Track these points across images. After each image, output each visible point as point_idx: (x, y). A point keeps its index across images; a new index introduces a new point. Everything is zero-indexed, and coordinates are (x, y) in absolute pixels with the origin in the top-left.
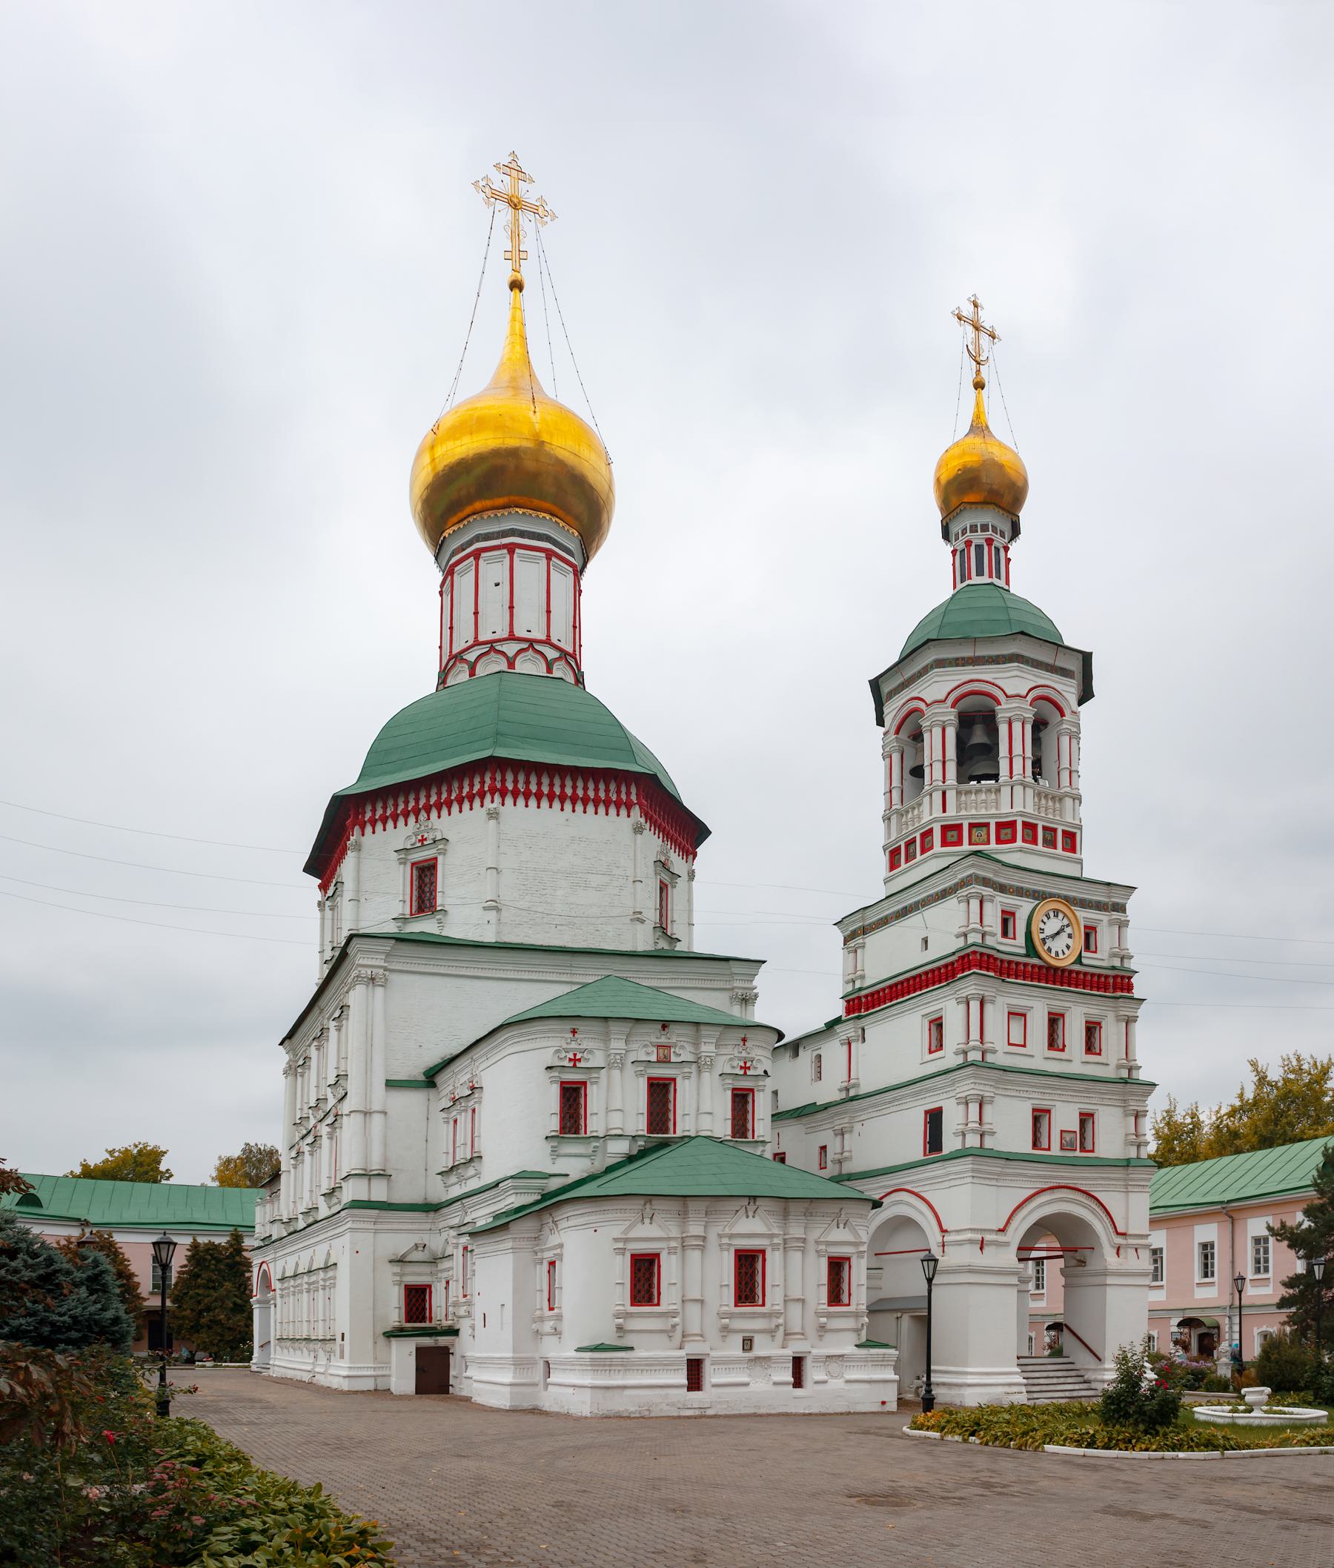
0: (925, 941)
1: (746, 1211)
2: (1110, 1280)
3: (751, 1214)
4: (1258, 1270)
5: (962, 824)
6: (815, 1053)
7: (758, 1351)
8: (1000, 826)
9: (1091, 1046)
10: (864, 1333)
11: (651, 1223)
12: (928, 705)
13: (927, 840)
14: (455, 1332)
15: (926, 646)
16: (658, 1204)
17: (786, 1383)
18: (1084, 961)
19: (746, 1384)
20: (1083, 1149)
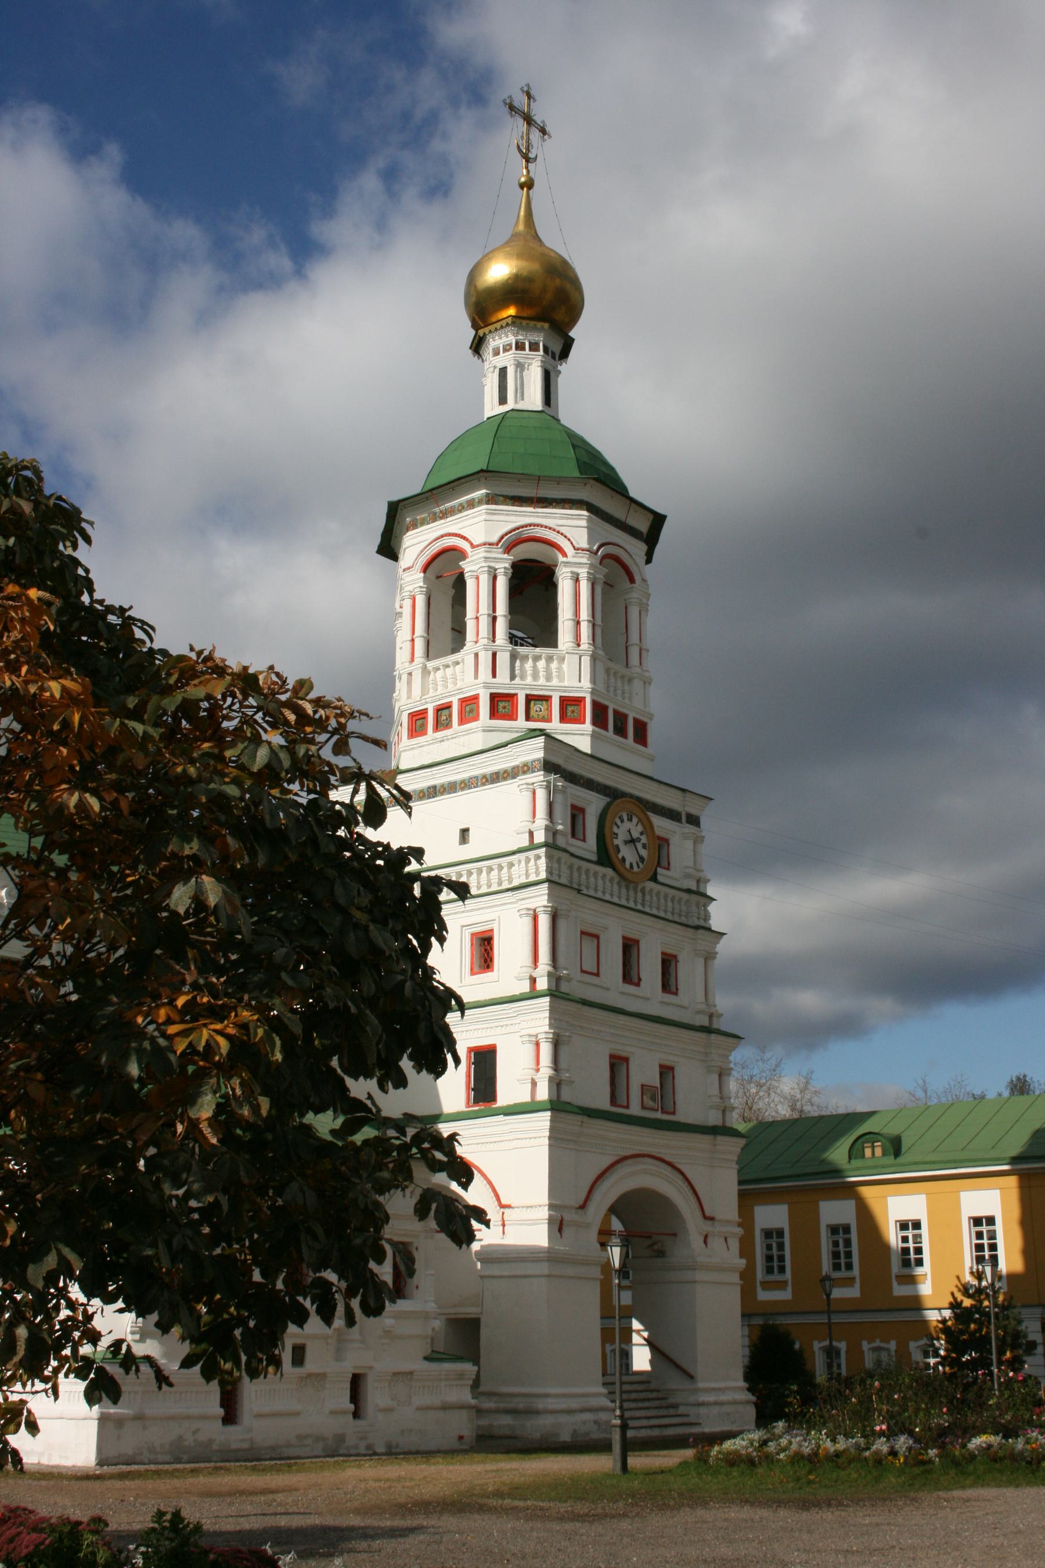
0: (464, 833)
2: (699, 1276)
4: (769, 1270)
5: (516, 695)
7: (311, 1365)
8: (565, 702)
9: (668, 985)
12: (473, 546)
17: (343, 1412)
18: (660, 878)
19: (296, 1414)
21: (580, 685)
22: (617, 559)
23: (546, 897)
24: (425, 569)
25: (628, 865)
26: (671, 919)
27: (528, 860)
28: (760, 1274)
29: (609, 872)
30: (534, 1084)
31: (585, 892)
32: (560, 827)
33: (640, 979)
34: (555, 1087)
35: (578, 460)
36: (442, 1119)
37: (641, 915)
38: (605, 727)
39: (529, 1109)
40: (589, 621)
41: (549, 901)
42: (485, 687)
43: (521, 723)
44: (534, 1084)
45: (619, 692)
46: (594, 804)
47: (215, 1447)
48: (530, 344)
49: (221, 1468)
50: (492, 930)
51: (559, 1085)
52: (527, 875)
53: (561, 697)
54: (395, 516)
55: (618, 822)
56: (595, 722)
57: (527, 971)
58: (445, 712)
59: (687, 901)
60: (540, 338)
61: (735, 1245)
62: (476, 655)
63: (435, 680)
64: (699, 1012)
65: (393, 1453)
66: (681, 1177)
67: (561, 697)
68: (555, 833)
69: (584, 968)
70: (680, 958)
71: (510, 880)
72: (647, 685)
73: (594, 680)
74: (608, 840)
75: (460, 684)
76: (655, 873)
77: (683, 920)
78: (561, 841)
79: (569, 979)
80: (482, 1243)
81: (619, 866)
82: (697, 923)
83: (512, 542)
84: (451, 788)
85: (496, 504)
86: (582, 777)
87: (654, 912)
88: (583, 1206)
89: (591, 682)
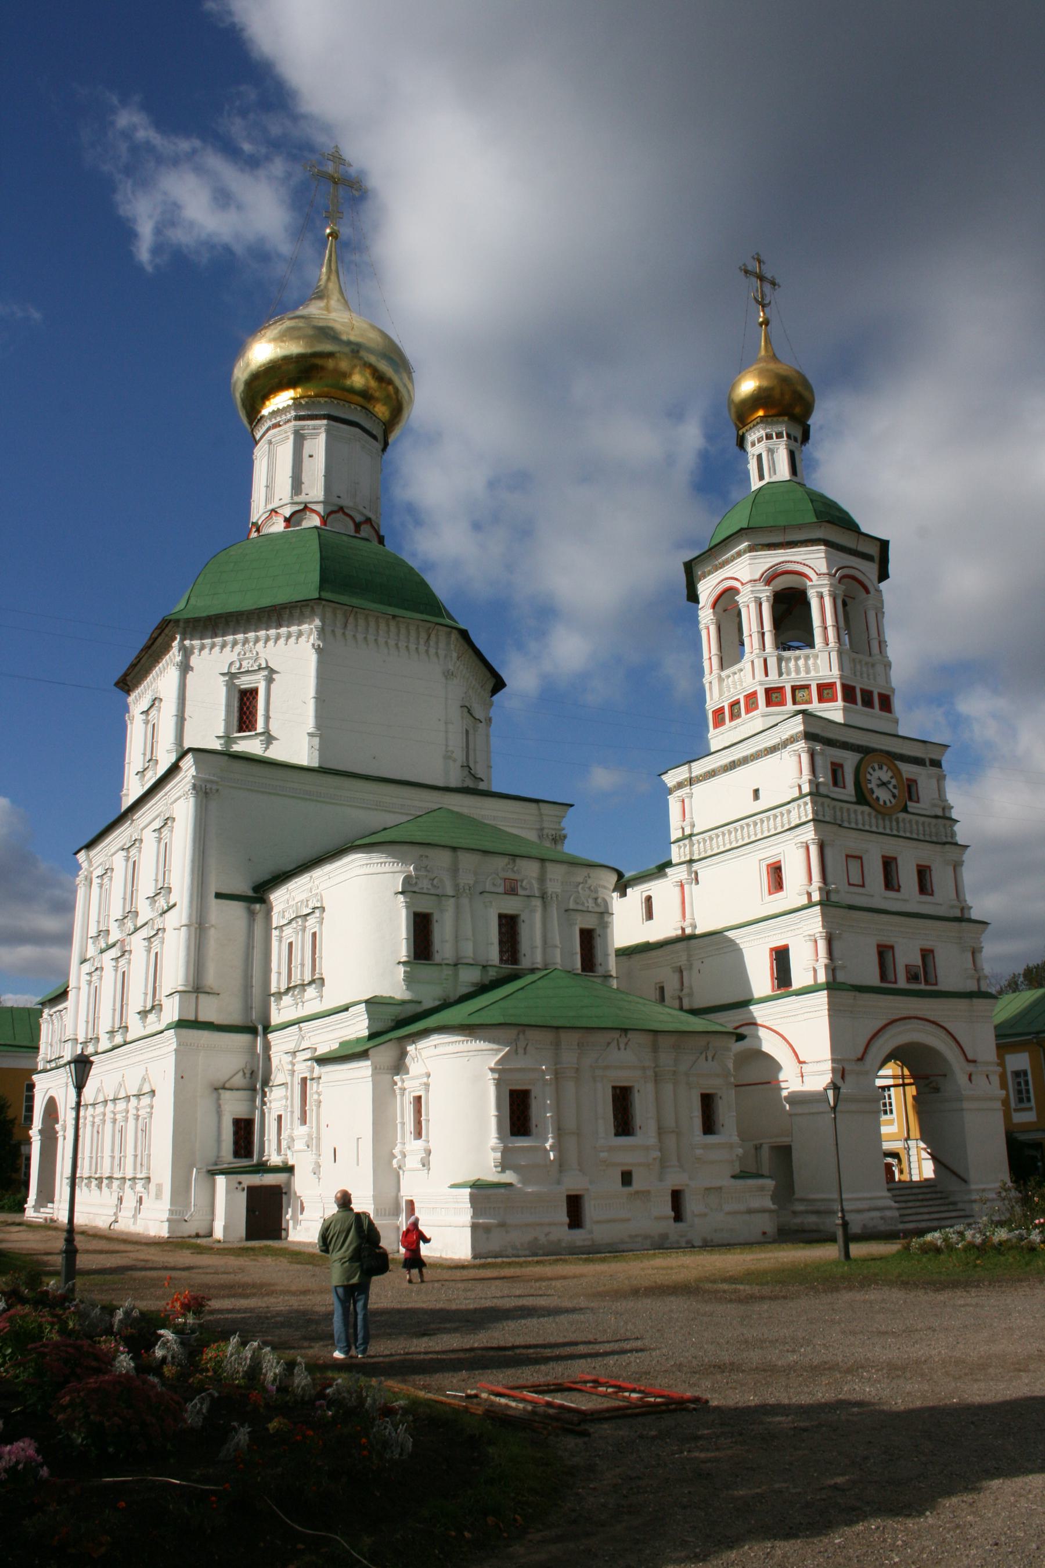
0: (756, 792)
1: (618, 1044)
3: (622, 1046)
4: (1021, 1100)
5: (784, 687)
6: (645, 894)
7: (637, 1184)
8: (821, 687)
10: (737, 1164)
11: (525, 1053)
12: (743, 584)
13: (751, 701)
14: (289, 1169)
15: (739, 534)
16: (531, 1034)
17: (666, 1218)
18: (910, 809)
20: (927, 982)
21: (831, 673)
22: (853, 578)
23: (813, 832)
24: (714, 606)
25: (881, 802)
26: (929, 840)
27: (799, 806)
28: (1013, 1105)
29: (866, 809)
30: (815, 970)
31: (846, 824)
32: (821, 780)
33: (899, 887)
34: (831, 972)
35: (815, 510)
36: (752, 1002)
37: (896, 839)
38: (855, 702)
39: (813, 989)
40: (833, 626)
41: (815, 835)
42: (761, 685)
43: (790, 707)
44: (815, 970)
45: (865, 675)
46: (849, 760)
47: (564, 1245)
48: (776, 434)
49: (561, 1260)
50: (780, 861)
51: (834, 970)
52: (800, 817)
53: (818, 684)
54: (692, 572)
55: (871, 771)
56: (845, 699)
57: (804, 889)
58: (737, 706)
59: (936, 824)
60: (783, 429)
61: (995, 1080)
62: (752, 662)
63: (728, 684)
64: (953, 907)
65: (708, 1245)
66: (945, 1032)
67: (818, 684)
68: (818, 785)
69: (851, 882)
70: (933, 868)
71: (789, 822)
72: (888, 668)
73: (841, 668)
74: (863, 785)
75: (744, 685)
76: (906, 806)
77: (934, 839)
78: (823, 790)
79: (837, 891)
80: (789, 1090)
81: (872, 802)
82: (944, 840)
83: (770, 578)
84: (745, 761)
85: (757, 551)
86: (837, 741)
87: (908, 835)
88: (861, 1059)
89: (839, 670)
